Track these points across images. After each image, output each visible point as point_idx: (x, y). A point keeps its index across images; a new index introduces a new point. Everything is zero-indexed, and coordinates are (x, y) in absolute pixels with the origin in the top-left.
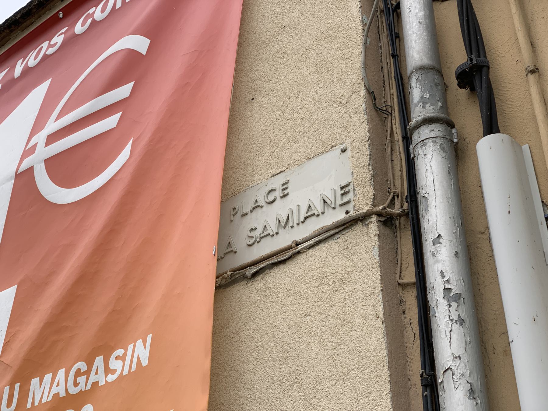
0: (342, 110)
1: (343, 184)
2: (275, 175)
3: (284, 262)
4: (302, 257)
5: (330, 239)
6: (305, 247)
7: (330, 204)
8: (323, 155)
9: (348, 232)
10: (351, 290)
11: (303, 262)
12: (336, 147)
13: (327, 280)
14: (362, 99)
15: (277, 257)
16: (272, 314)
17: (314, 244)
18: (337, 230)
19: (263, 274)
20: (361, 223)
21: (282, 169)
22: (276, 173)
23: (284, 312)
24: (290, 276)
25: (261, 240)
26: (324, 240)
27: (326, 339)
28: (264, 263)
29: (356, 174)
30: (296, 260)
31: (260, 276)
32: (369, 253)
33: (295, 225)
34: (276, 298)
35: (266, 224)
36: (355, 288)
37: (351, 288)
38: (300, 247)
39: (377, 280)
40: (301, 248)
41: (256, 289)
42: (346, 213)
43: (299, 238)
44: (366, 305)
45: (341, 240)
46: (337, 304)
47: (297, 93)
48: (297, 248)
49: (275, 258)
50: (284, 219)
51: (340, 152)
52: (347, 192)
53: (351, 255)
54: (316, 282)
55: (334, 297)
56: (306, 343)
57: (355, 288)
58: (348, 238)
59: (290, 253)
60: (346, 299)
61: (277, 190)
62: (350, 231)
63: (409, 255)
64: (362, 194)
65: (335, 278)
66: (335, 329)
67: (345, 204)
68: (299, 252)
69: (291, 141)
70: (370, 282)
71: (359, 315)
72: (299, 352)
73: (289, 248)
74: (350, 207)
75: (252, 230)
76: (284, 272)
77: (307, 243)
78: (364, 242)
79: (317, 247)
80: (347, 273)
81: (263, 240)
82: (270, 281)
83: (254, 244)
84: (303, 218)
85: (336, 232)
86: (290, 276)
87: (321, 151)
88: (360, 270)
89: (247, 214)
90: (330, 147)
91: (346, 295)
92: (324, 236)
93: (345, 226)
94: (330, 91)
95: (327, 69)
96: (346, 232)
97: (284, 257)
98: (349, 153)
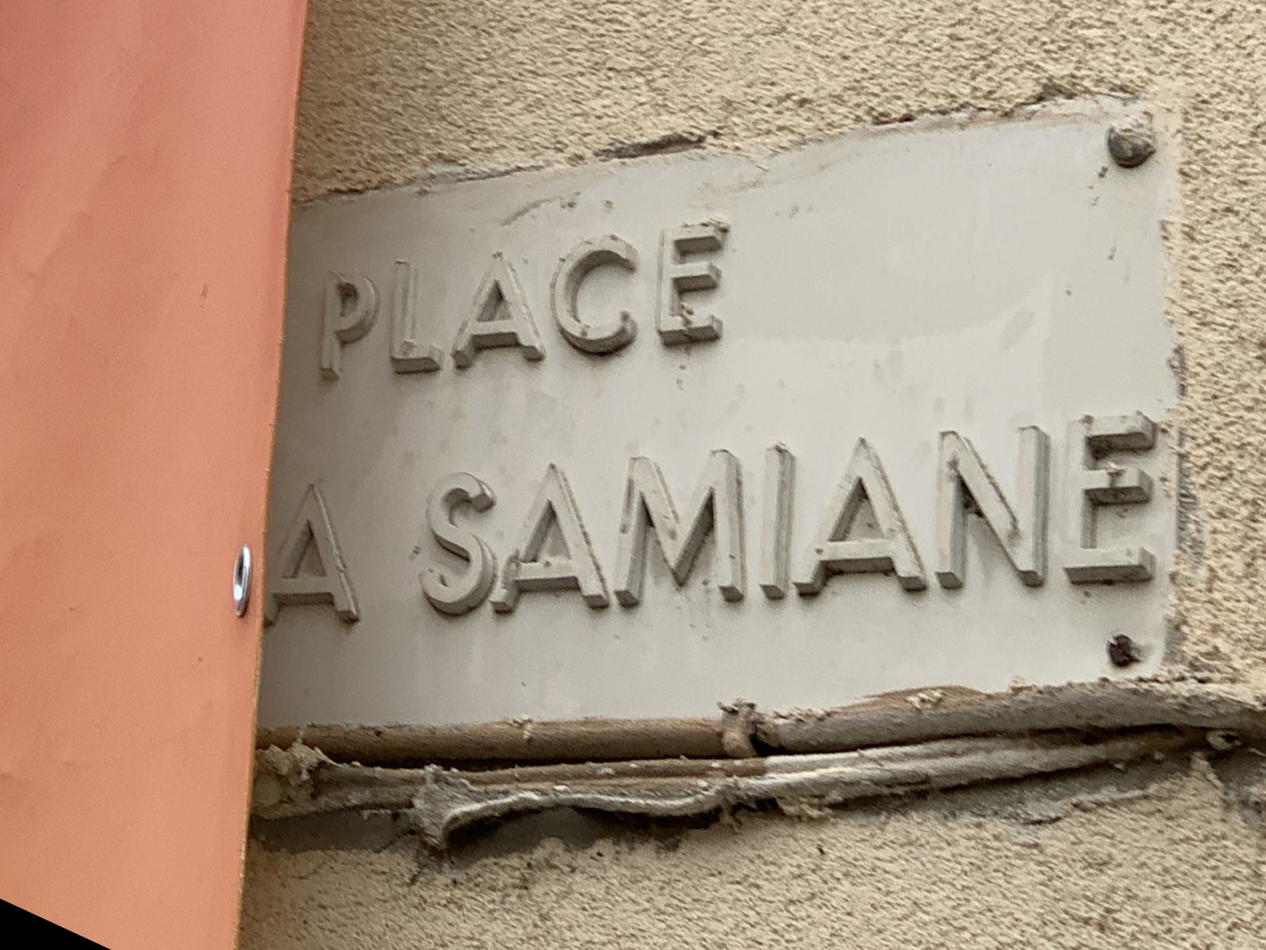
1: (1110, 424)
5: (990, 800)
6: (815, 783)
8: (972, 131)
9: (1115, 804)
11: (798, 890)
20: (1212, 777)
21: (679, 124)
31: (503, 862)
35: (552, 494)
38: (777, 768)
48: (761, 772)
49: (609, 776)
58: (1114, 851)
67: (1109, 583)
76: (661, 902)
77: (827, 765)
78: (1224, 925)
79: (899, 826)
82: (570, 928)
90: (1031, 89)
93: (1097, 752)
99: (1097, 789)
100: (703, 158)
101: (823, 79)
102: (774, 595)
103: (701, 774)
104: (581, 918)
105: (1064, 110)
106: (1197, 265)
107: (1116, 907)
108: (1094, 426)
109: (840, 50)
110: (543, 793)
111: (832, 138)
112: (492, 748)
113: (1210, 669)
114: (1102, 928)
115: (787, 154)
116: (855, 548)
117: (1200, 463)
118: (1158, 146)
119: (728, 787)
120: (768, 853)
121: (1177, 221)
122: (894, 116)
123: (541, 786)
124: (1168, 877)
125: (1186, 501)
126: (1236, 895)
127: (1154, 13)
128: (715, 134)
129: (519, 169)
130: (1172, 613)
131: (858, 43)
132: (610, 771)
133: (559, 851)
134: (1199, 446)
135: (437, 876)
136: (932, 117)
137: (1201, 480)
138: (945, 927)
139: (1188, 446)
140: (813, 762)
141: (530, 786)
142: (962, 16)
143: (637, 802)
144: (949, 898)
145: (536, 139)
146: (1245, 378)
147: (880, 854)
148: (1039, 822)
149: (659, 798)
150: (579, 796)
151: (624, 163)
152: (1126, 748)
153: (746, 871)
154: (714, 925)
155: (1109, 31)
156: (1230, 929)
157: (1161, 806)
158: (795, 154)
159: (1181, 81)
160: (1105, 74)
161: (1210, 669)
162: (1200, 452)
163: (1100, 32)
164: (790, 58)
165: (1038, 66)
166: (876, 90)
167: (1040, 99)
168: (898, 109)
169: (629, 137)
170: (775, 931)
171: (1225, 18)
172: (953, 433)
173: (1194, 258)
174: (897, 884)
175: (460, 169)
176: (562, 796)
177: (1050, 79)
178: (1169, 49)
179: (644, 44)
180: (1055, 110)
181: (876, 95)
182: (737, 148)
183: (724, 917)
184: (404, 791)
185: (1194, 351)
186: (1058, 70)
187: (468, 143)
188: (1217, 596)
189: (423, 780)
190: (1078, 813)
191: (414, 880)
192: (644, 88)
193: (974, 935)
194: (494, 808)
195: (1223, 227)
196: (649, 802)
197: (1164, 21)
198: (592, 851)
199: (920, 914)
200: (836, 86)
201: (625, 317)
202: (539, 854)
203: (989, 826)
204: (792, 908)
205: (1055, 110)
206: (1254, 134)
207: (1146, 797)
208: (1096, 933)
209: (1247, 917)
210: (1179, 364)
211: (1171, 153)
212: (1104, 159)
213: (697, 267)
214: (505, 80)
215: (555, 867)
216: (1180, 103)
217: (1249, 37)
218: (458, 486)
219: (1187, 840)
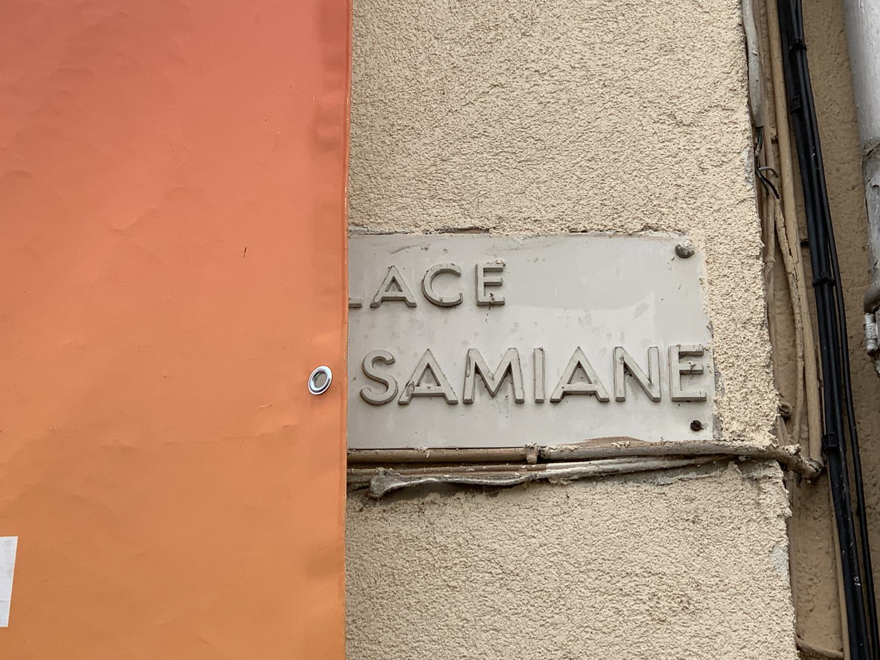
0: (675, 136)
2: (455, 229)
4: (550, 498)
5: (642, 477)
6: (569, 473)
7: (646, 386)
8: (615, 239)
9: (697, 479)
10: (707, 633)
11: (557, 511)
13: (633, 584)
14: (740, 137)
15: (476, 471)
16: (454, 621)
17: (595, 474)
18: (667, 464)
19: (422, 500)
20: (738, 470)
22: (456, 226)
23: (494, 630)
24: (513, 536)
25: (410, 400)
26: (623, 474)
28: (437, 472)
30: (532, 497)
31: (409, 502)
32: (760, 557)
34: (464, 581)
35: (428, 360)
36: (720, 633)
38: (551, 468)
39: (783, 633)
40: (557, 474)
41: (398, 537)
43: (553, 444)
45: (675, 493)
47: (523, 21)
48: (544, 469)
50: (494, 370)
51: (673, 255)
52: (697, 371)
53: (706, 541)
54: (596, 579)
55: (655, 635)
57: (720, 633)
58: (697, 495)
59: (521, 474)
60: (691, 653)
61: (462, 276)
62: (704, 478)
63: (815, 580)
64: (737, 391)
65: (657, 587)
67: (689, 401)
70: (765, 631)
75: (379, 360)
76: (490, 516)
77: (574, 466)
78: (745, 521)
79: (601, 487)
80: (694, 586)
82: (445, 527)
83: (386, 403)
84: (561, 394)
85: (664, 467)
86: (513, 536)
87: (611, 224)
88: (734, 591)
90: (639, 227)
91: (692, 642)
93: (692, 461)
94: (637, 65)
97: (501, 479)
98: (699, 265)
100: (490, 237)
101: (543, 212)
102: (539, 402)
103: (517, 470)
104: (451, 523)
105: (654, 235)
106: (714, 293)
107: (699, 515)
108: (681, 348)
109: (551, 203)
110: (440, 478)
111: (552, 235)
113: (744, 436)
114: (694, 522)
115: (531, 239)
117: (721, 361)
118: (696, 252)
120: (541, 497)
121: (706, 278)
122: (579, 230)
123: (439, 475)
124: (720, 504)
125: (717, 374)
126: (749, 510)
127: (690, 206)
128: (494, 228)
129: (396, 232)
131: (559, 201)
133: (438, 498)
134: (720, 355)
135: (374, 508)
136: (595, 232)
137: (722, 366)
138: (626, 524)
139: (716, 355)
140: (561, 466)
141: (433, 475)
142: (605, 197)
144: (626, 513)
145: (404, 221)
146: (737, 333)
147: (594, 497)
149: (495, 479)
150: (458, 479)
151: (452, 236)
152: (701, 460)
153: (532, 504)
154: (517, 525)
155: (671, 210)
156: (747, 522)
157: (716, 479)
158: (534, 239)
159: (703, 231)
160: (671, 225)
161: (744, 436)
162: (721, 357)
163: (667, 210)
164: (528, 203)
165: (641, 219)
166: (570, 220)
167: (642, 230)
169: (452, 225)
170: (547, 527)
171: (718, 210)
172: (621, 347)
173: (712, 291)
174: (602, 509)
176: (449, 480)
177: (647, 224)
178: (697, 219)
180: (650, 235)
181: (571, 222)
182: (507, 235)
183: (522, 521)
184: (365, 479)
186: (651, 221)
187: (368, 219)
188: (732, 407)
189: (377, 474)
190: (680, 482)
191: (361, 510)
192: (457, 207)
193: (638, 526)
195: (723, 281)
196: (492, 481)
197: (693, 209)
198: (455, 497)
199: (613, 518)
200: (551, 216)
201: (461, 295)
202: (428, 499)
203: (642, 487)
204: (555, 518)
205: (650, 235)
206: (734, 251)
207: (710, 477)
208: (692, 524)
209: (754, 517)
210: (710, 327)
211: (701, 254)
213: (493, 278)
214: (385, 196)
215: (436, 504)
216: (703, 238)
217: (729, 218)
218: (383, 356)
219: (727, 491)
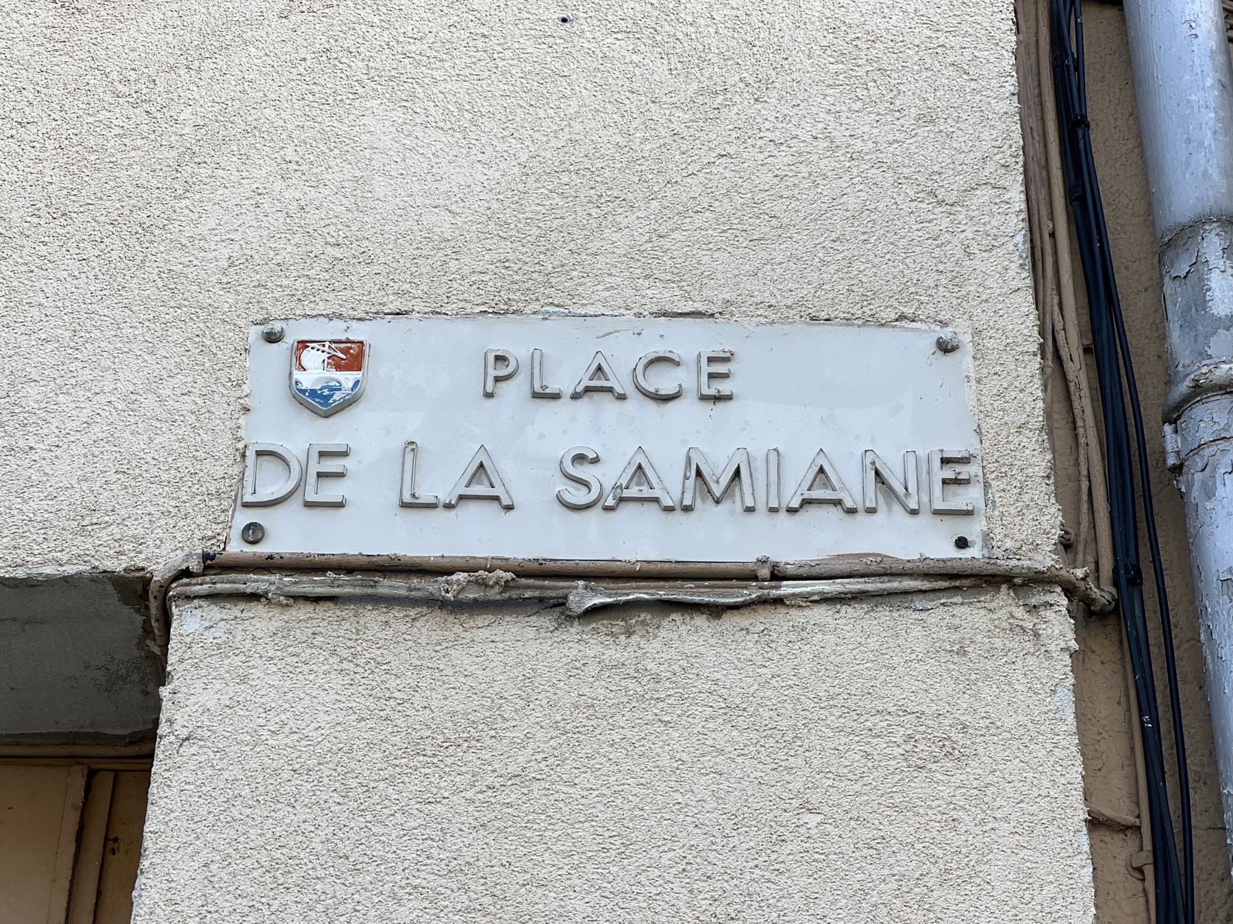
1: (953, 451)
3: (716, 611)
4: (778, 620)
5: (896, 601)
9: (962, 604)
10: (975, 784)
12: (913, 325)
15: (697, 587)
21: (700, 307)
25: (618, 505)
27: (882, 906)
29: (990, 436)
33: (761, 507)
35: (640, 459)
37: (975, 779)
38: (787, 586)
42: (963, 548)
44: (1029, 847)
46: (921, 811)
47: (756, 85)
48: (778, 588)
49: (691, 588)
56: (801, 894)
66: (917, 885)
68: (779, 601)
69: (737, 229)
71: (1005, 871)
72: (775, 915)
73: (747, 576)
74: (973, 529)
79: (847, 611)
81: (627, 510)
85: (924, 588)
89: (556, 396)
90: (893, 316)
92: (880, 586)
95: (876, 62)
96: (955, 600)
97: (732, 596)
98: (964, 360)
99: (951, 597)
102: (773, 510)
103: (745, 588)
108: (944, 453)
112: (553, 571)
116: (818, 494)
119: (764, 595)
129: (603, 315)
130: (985, 529)
131: (797, 286)
132: (692, 586)
143: (696, 599)
148: (922, 610)
152: (966, 582)
158: (768, 326)
162: (991, 466)
168: (823, 315)
175: (567, 311)
179: (676, 271)
185: (984, 427)
186: (908, 311)
194: (620, 601)
204: (790, 645)
205: (906, 325)
207: (979, 601)
210: (979, 431)
212: (934, 348)
